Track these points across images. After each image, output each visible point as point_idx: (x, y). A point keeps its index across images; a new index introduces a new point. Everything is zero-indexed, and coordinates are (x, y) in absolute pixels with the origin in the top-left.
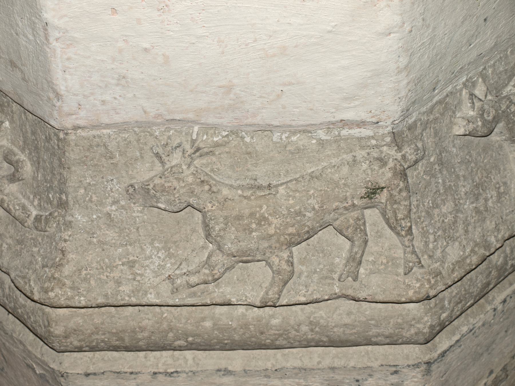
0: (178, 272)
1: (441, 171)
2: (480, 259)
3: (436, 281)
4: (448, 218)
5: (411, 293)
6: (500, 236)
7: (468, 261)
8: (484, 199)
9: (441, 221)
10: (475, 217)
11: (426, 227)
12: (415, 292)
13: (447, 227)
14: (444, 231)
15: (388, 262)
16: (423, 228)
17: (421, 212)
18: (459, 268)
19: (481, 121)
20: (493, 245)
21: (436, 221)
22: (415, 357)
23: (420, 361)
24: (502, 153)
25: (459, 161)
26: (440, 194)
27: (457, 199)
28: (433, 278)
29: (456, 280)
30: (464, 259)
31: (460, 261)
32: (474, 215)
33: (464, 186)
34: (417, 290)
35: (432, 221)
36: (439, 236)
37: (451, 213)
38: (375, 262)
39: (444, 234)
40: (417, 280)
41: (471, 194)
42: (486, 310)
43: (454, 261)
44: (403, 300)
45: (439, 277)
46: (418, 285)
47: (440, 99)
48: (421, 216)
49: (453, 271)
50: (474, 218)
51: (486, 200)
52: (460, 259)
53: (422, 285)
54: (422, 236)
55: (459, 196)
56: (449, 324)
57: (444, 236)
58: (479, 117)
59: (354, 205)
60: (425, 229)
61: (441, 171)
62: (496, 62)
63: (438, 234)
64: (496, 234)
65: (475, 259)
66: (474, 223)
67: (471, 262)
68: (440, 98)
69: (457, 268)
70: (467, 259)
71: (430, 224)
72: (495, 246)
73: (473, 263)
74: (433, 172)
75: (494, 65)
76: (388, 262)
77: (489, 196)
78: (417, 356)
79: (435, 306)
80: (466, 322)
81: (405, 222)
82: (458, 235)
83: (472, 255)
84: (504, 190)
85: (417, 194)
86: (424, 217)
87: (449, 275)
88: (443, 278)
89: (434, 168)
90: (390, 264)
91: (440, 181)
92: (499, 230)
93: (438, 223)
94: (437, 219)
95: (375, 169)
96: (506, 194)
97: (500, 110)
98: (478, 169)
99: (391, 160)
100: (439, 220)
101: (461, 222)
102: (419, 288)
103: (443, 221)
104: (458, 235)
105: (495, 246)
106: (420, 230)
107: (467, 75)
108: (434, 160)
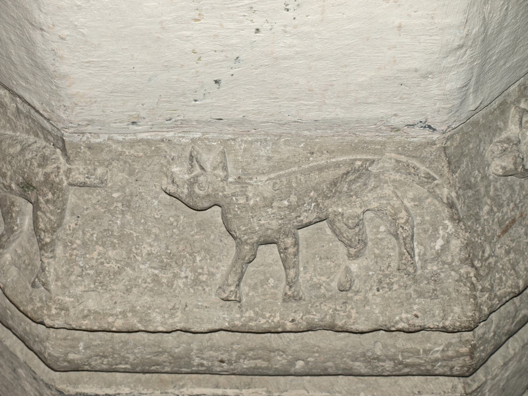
0: (520, 209)
1: (123, 213)
2: (126, 326)
3: (57, 314)
4: (110, 264)
5: (29, 308)
6: (171, 321)
7: (110, 319)
8: (174, 273)
9: (99, 261)
10: (149, 283)
11: (76, 256)
12: (33, 309)
13: (104, 272)
14: (98, 274)
15: (29, 265)
16: (71, 255)
17: (77, 238)
18: (94, 318)
19: (188, 189)
20: (155, 325)
21: (93, 258)
22: (51, 377)
23: (53, 384)
24: (226, 242)
25: (156, 217)
26: (112, 235)
27: (133, 253)
28: (56, 308)
29: (84, 327)
30: (106, 315)
31: (100, 313)
32: (149, 280)
33: (151, 246)
34: (36, 309)
35: (88, 256)
36: (89, 274)
37: (117, 261)
38: (20, 257)
39: (96, 277)
40: (40, 300)
41: (156, 257)
42: (166, 391)
43: (93, 308)
44: (22, 309)
45: (63, 312)
46: (39, 305)
47: (149, 139)
48: (75, 242)
49: (85, 317)
50: (147, 284)
51: (176, 276)
52: (101, 311)
53: (41, 307)
54: (65, 262)
55: (139, 251)
56: (87, 370)
57: (95, 278)
58: (188, 184)
59: (10, 187)
60: (74, 257)
61: (123, 213)
62: (257, 141)
63: (89, 272)
64: (167, 316)
65: (119, 324)
66: (145, 288)
67: (114, 322)
68: (149, 137)
69: (92, 317)
70: (111, 317)
71: (83, 256)
72: (157, 327)
73: (116, 324)
74: (112, 208)
75: (251, 143)
76: (29, 265)
77: (183, 275)
78: (54, 378)
79: (64, 339)
80: (132, 385)
81: (45, 236)
82: (114, 287)
83: (120, 316)
84: (207, 279)
85: (78, 217)
86: (79, 246)
87: (78, 318)
88: (68, 315)
89: (115, 205)
90: (30, 267)
91: (119, 222)
92: (172, 316)
93: (94, 261)
94: (95, 257)
95: (34, 164)
96: (207, 286)
97: (222, 192)
98: (182, 239)
99: (55, 165)
100: (97, 259)
101: (127, 278)
102: (38, 308)
103: (102, 263)
104: (114, 287)
105: (157, 327)
106: (68, 255)
107: (204, 133)
108: (119, 197)
